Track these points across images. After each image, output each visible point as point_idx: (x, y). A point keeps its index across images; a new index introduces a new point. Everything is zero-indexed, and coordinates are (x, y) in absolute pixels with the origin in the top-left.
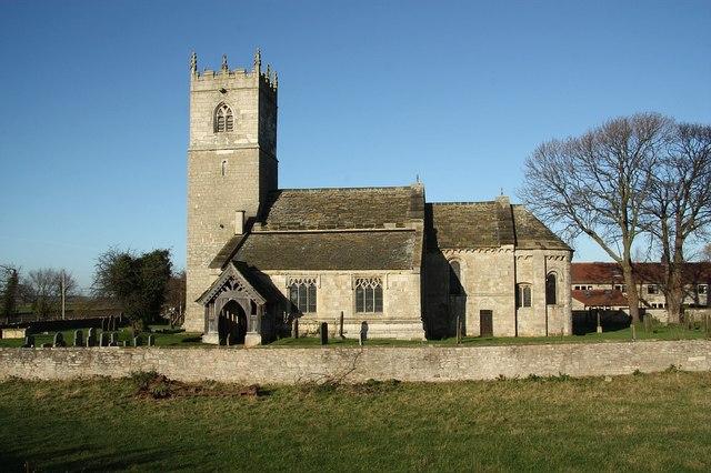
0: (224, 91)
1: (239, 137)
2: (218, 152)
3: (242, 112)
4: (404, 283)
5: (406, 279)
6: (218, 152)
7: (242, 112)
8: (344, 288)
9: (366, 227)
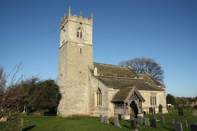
0: (81, 23)
1: (86, 41)
3: (87, 32)
4: (162, 95)
5: (162, 94)
6: (79, 45)
7: (87, 32)
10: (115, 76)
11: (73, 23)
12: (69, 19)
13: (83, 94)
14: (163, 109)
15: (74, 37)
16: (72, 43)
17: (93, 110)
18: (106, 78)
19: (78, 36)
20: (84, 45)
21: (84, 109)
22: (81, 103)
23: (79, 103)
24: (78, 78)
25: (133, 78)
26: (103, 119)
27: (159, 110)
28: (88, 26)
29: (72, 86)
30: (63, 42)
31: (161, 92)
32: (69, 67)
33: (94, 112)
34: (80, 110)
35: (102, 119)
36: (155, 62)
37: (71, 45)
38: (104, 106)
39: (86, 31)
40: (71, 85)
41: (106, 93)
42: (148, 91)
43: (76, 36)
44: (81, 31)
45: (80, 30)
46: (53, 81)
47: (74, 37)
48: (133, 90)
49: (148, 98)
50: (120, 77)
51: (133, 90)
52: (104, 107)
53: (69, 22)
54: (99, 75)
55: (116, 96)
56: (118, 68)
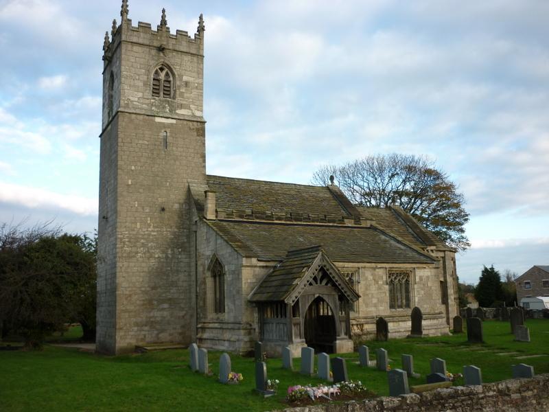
1: (181, 106)
2: (158, 120)
3: (185, 78)
4: (428, 277)
5: (429, 274)
6: (158, 120)
7: (185, 78)
8: (380, 282)
9: (329, 222)
10: (279, 219)
11: (136, 48)
12: (124, 38)
13: (175, 279)
14: (424, 323)
15: (140, 95)
16: (133, 116)
17: (203, 329)
18: (248, 225)
19: (156, 92)
20: (174, 121)
21: (178, 327)
22: (166, 306)
23: (161, 307)
24: (154, 227)
25: (342, 221)
26: (529, 357)
27: (377, 328)
28: (187, 58)
29: (137, 253)
30: (109, 113)
31: (424, 265)
32: (125, 193)
33: (205, 336)
34: (163, 331)
35: (527, 359)
36: (431, 167)
37: (131, 121)
38: (232, 314)
39: (181, 76)
40: (134, 249)
41: (237, 274)
42: (379, 265)
43: (149, 94)
44: (167, 74)
45: (164, 72)
46: (76, 239)
47: (140, 95)
48: (317, 262)
49: (380, 288)
50: (296, 220)
51: (317, 262)
52: (232, 320)
53: (123, 46)
54: (222, 216)
55: (264, 284)
56: (293, 193)
